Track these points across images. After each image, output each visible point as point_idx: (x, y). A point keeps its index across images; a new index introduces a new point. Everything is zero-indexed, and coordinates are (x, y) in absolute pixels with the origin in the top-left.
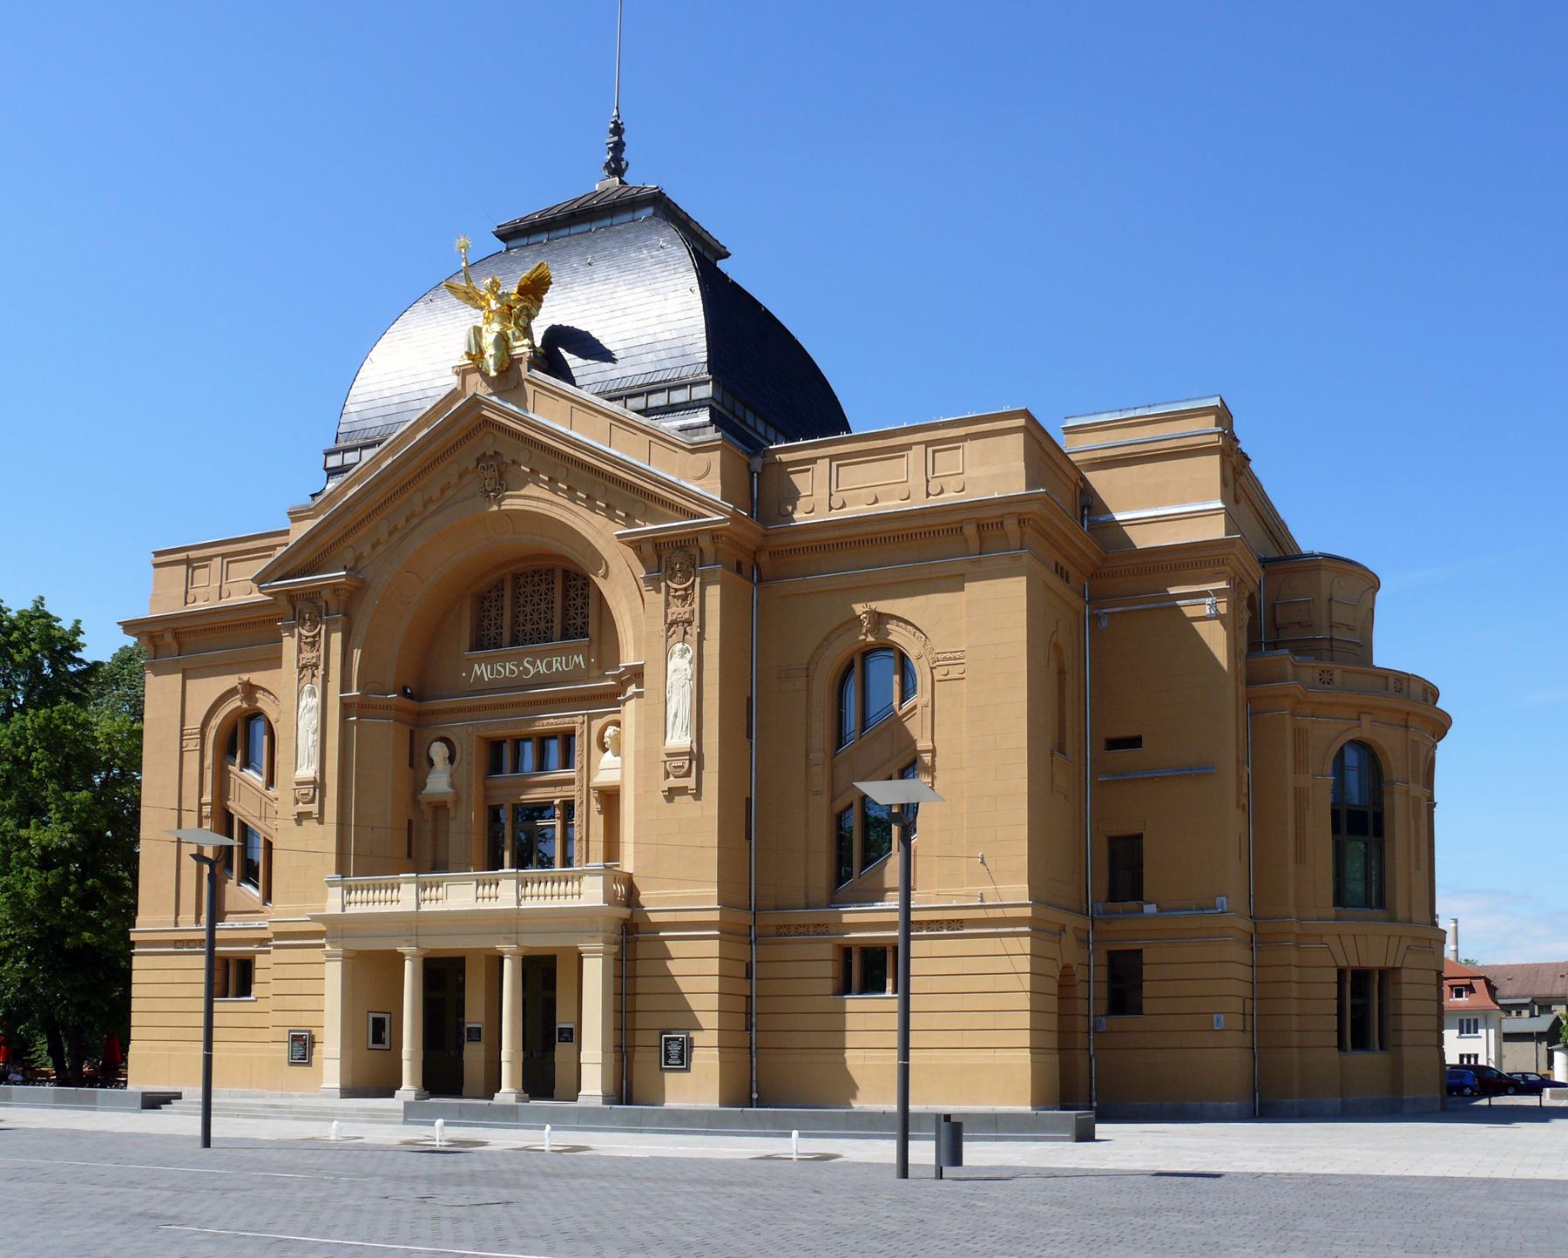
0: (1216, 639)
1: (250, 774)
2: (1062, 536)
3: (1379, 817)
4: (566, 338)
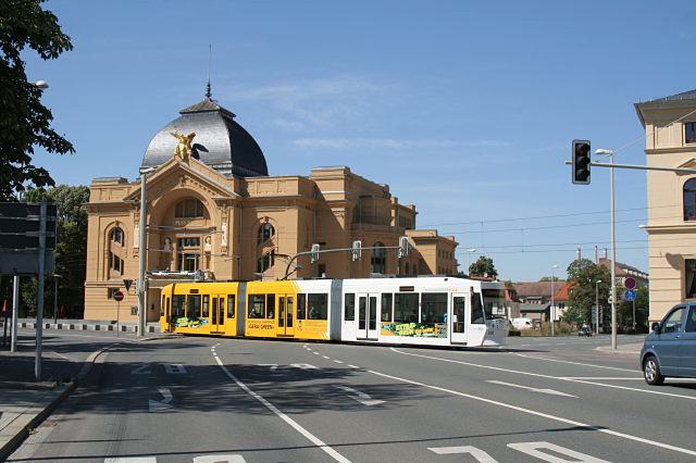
0: (342, 221)
1: (117, 243)
2: (309, 199)
3: (384, 259)
4: (197, 146)
